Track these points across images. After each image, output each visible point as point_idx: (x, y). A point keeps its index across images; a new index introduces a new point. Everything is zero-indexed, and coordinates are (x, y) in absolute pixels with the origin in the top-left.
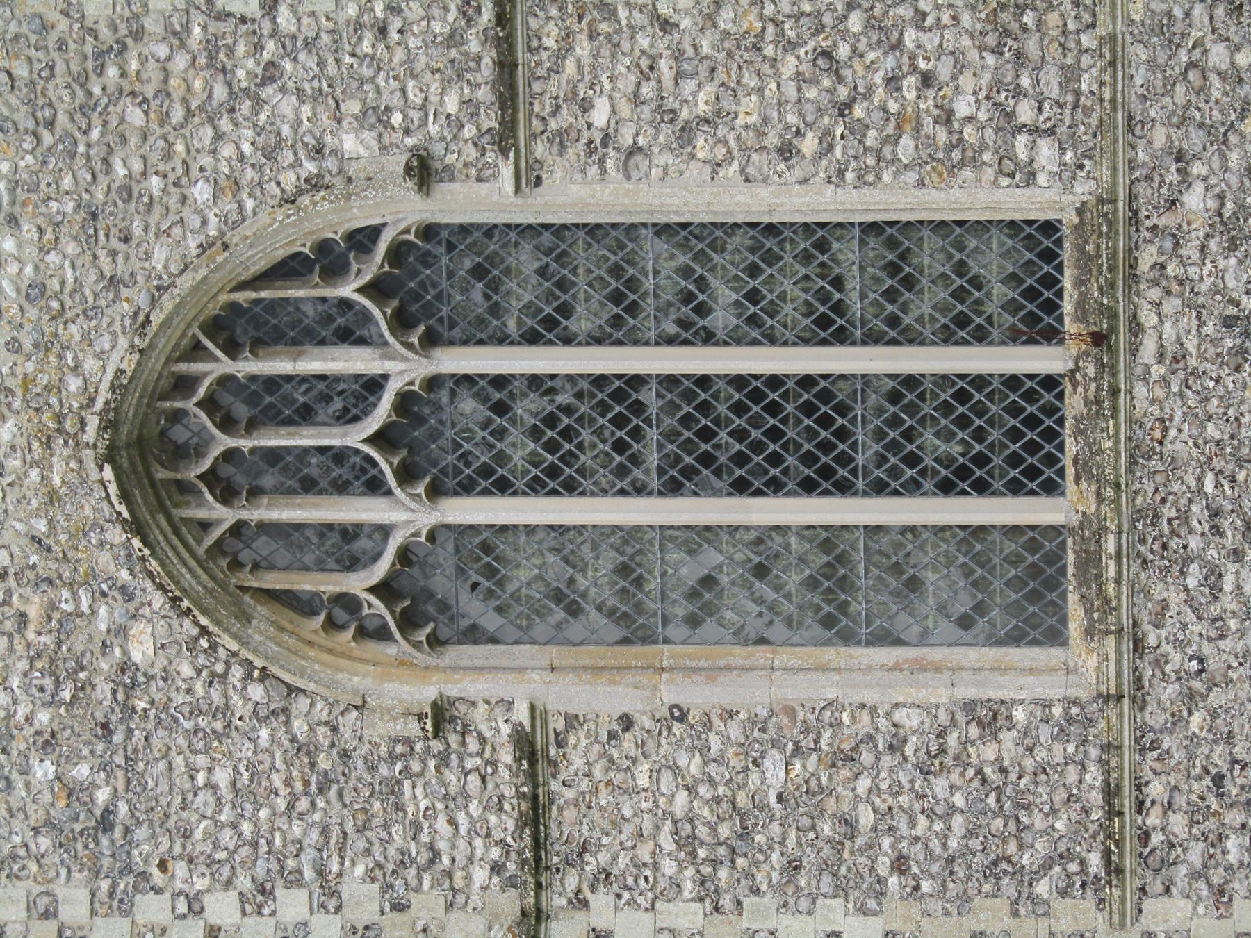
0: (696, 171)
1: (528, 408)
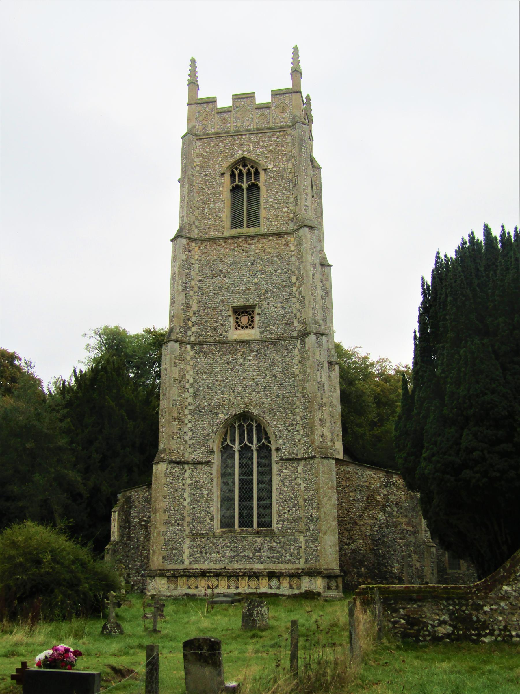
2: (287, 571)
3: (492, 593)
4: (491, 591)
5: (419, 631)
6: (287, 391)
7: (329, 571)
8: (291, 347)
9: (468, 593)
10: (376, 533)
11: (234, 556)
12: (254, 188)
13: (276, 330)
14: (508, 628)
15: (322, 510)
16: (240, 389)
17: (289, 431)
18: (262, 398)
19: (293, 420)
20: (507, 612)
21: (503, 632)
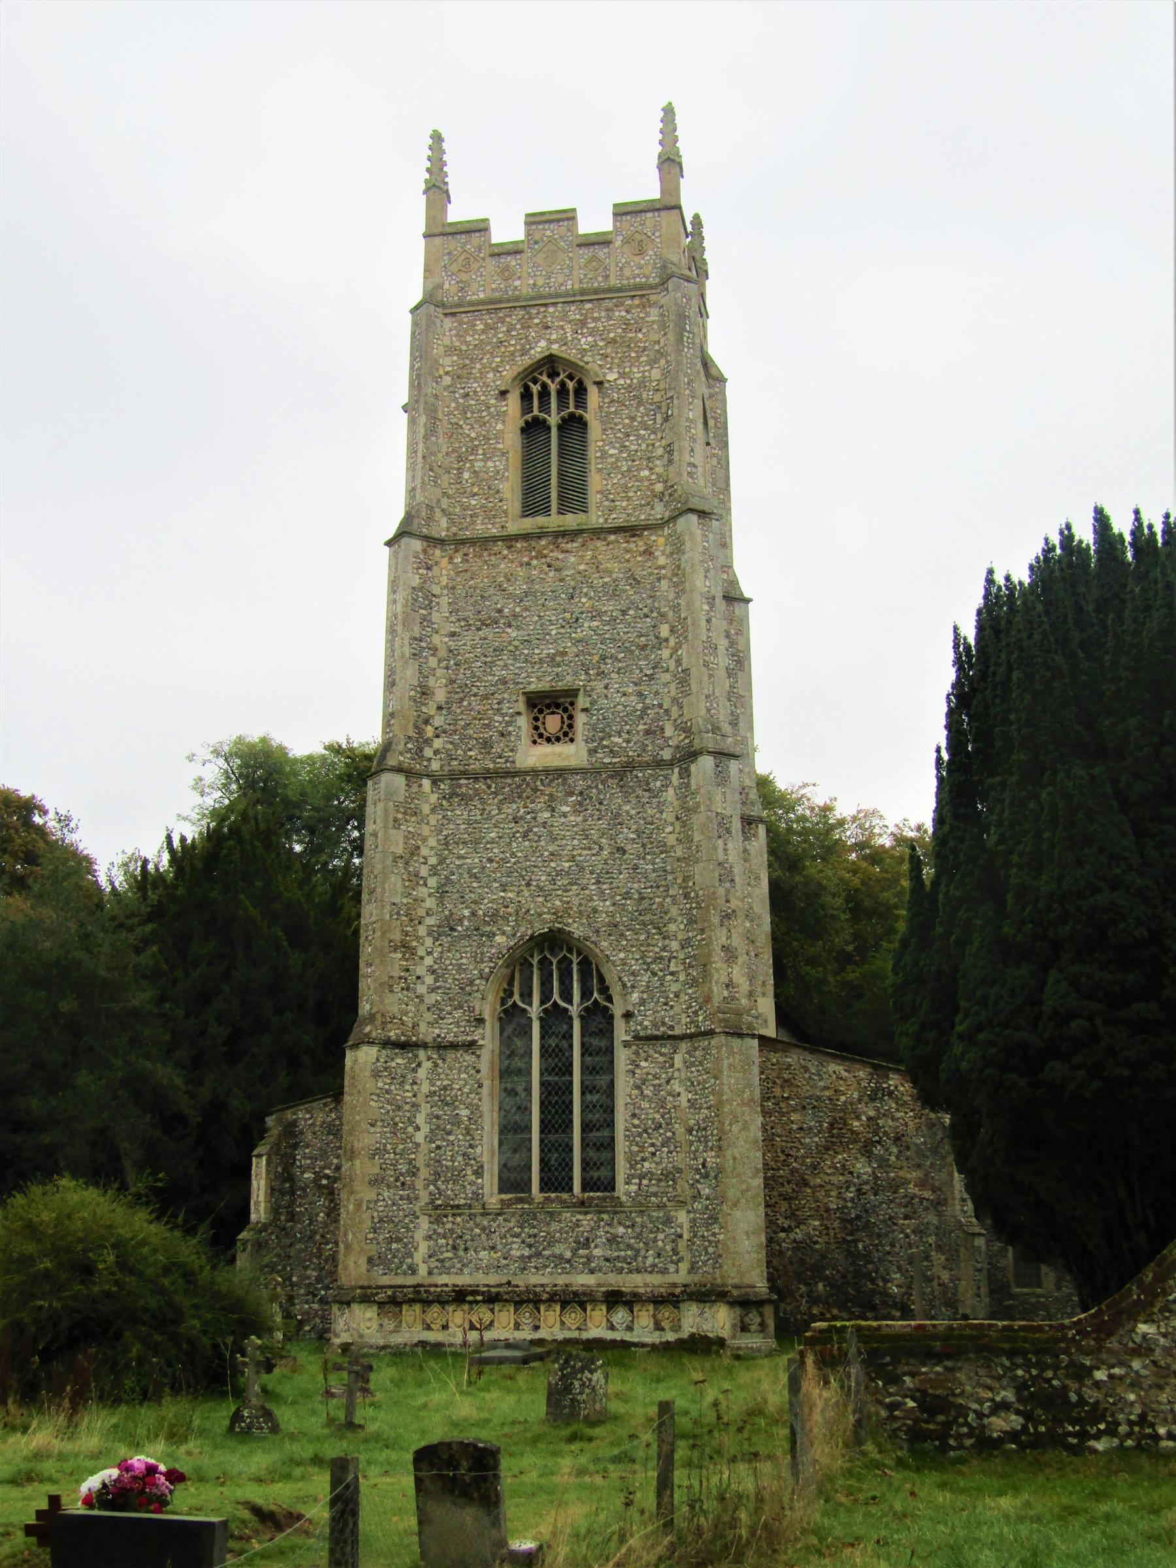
2: (649, 1290)
3: (1113, 1339)
4: (1110, 1334)
5: (947, 1425)
6: (649, 884)
7: (743, 1291)
8: (658, 784)
9: (1058, 1340)
10: (849, 1205)
11: (530, 1257)
12: (574, 425)
13: (624, 745)
14: (1150, 1418)
15: (729, 1153)
16: (543, 878)
17: (654, 974)
18: (592, 900)
19: (664, 949)
20: (1146, 1383)
21: (1136, 1429)
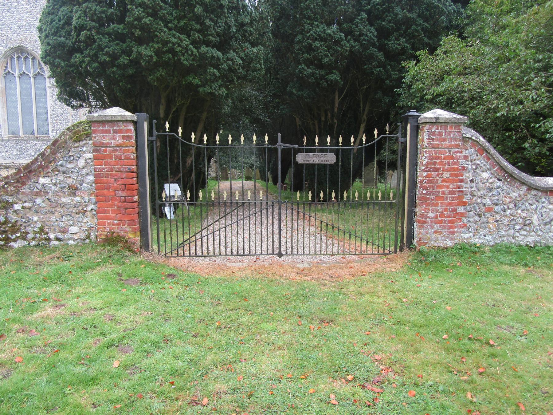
0: (51, 102)
1: (45, 123)
3: (26, 187)
4: (23, 184)
11: (20, 155)
14: (45, 230)
16: (16, 27)
18: (34, 37)
21: (38, 235)
